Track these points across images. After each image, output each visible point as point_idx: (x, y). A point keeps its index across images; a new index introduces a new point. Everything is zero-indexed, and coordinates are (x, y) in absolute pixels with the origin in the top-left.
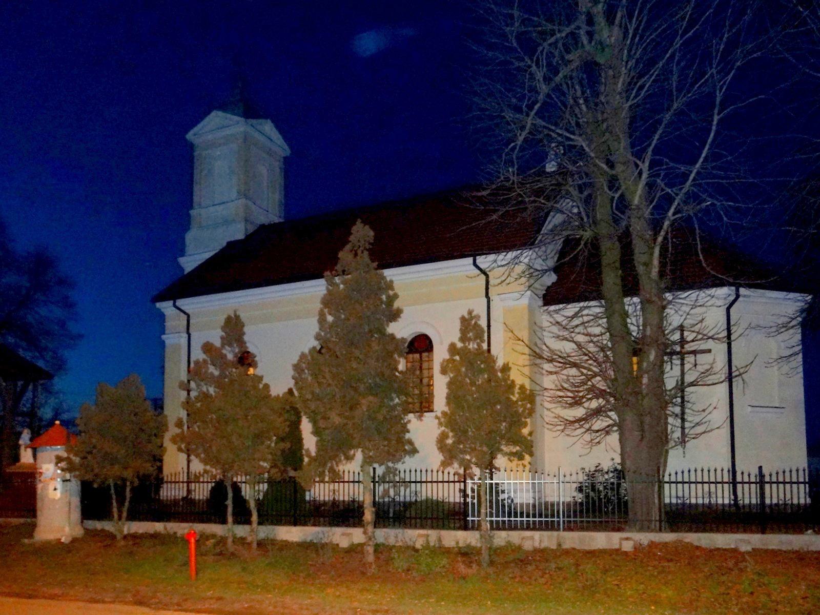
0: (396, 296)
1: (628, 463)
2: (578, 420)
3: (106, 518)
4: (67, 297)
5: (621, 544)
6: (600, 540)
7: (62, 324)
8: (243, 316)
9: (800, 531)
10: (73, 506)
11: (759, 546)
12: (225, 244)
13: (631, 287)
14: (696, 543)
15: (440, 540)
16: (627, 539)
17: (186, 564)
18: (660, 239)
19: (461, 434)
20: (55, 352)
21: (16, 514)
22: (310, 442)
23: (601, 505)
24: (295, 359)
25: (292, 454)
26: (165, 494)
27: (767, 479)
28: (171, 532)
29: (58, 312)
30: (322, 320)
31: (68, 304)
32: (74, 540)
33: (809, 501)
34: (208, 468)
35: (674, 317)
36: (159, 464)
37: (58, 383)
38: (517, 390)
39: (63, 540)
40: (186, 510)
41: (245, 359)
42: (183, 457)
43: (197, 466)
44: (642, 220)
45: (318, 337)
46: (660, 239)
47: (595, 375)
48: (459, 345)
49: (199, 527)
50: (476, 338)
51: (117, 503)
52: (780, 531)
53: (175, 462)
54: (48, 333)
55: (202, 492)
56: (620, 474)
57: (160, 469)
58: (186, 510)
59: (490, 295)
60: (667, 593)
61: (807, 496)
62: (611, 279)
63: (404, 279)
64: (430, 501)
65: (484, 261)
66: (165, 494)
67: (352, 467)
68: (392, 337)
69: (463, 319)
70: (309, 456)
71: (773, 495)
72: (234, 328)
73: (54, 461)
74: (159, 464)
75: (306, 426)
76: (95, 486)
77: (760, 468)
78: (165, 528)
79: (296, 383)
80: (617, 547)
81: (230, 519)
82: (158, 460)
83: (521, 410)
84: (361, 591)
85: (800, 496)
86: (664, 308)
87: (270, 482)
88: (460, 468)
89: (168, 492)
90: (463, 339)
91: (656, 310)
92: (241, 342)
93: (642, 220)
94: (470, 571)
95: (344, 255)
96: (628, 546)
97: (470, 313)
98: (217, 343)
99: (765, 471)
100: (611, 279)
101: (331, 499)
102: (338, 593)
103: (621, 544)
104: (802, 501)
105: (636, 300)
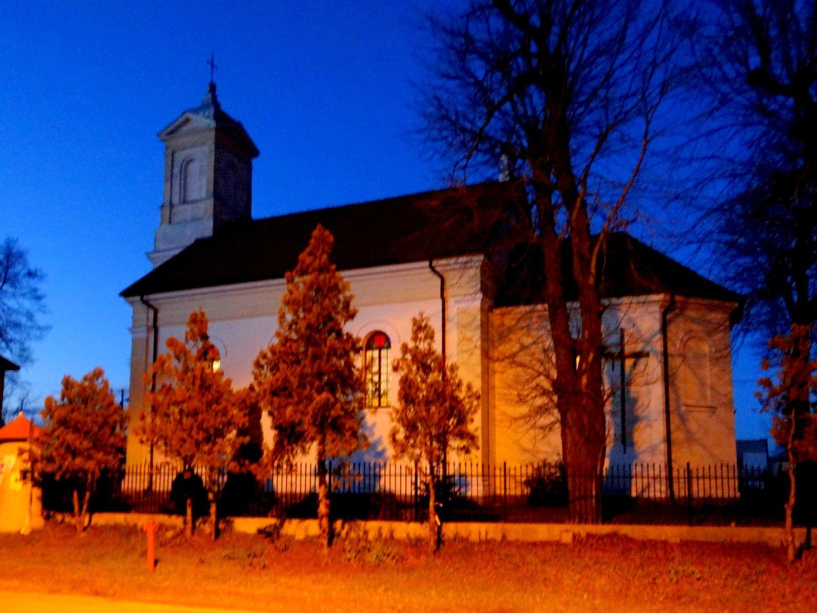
0: (351, 297)
1: (569, 459)
2: (524, 417)
3: (570, 520)
4: (35, 290)
5: (561, 536)
6: (542, 531)
7: (30, 316)
8: (207, 316)
9: (726, 523)
10: (34, 499)
11: (690, 538)
12: (193, 241)
13: (571, 291)
14: (630, 535)
15: (392, 533)
16: (567, 531)
17: (144, 554)
18: (596, 249)
19: (411, 427)
20: (22, 343)
21: (526, 517)
22: (269, 437)
23: (546, 496)
24: (255, 356)
25: (250, 450)
26: (126, 485)
27: (694, 475)
28: (131, 524)
29: (28, 304)
30: (282, 317)
31: (38, 297)
32: (33, 532)
33: (738, 494)
34: (168, 459)
35: (607, 323)
36: (120, 456)
37: (24, 374)
38: (464, 388)
39: (23, 531)
40: (147, 501)
41: (208, 353)
42: (146, 449)
43: (159, 458)
44: (66, 456)
45: (278, 334)
46: (596, 249)
47: (540, 374)
48: (411, 345)
49: (162, 518)
50: (426, 337)
51: (795, 414)
52: (713, 525)
53: (137, 453)
54: (17, 325)
55: (164, 483)
56: (562, 467)
57: (123, 461)
58: (147, 501)
59: (445, 295)
60: (601, 582)
61: (737, 490)
62: (552, 288)
63: (360, 284)
64: (298, 496)
65: (440, 264)
66: (126, 485)
67: (307, 459)
68: (349, 336)
69: (415, 322)
70: (268, 449)
71: (700, 489)
72: (198, 324)
73: (16, 452)
74: (120, 456)
75: (266, 421)
76: (57, 477)
77: (688, 464)
78: (125, 520)
79: (256, 378)
80: (557, 538)
81: (789, 522)
82: (121, 450)
83: (468, 407)
84: (314, 582)
85: (728, 489)
86: (601, 313)
87: (230, 474)
88: (411, 461)
89: (132, 483)
90: (415, 339)
91: (593, 316)
92: (205, 337)
93: (66, 456)
94: (418, 562)
95: (304, 257)
96: (567, 538)
97: (421, 314)
98: (182, 339)
99: (692, 466)
100: (552, 288)
101: (289, 490)
102: (291, 584)
103: (561, 536)
104: (732, 494)
105: (577, 305)
